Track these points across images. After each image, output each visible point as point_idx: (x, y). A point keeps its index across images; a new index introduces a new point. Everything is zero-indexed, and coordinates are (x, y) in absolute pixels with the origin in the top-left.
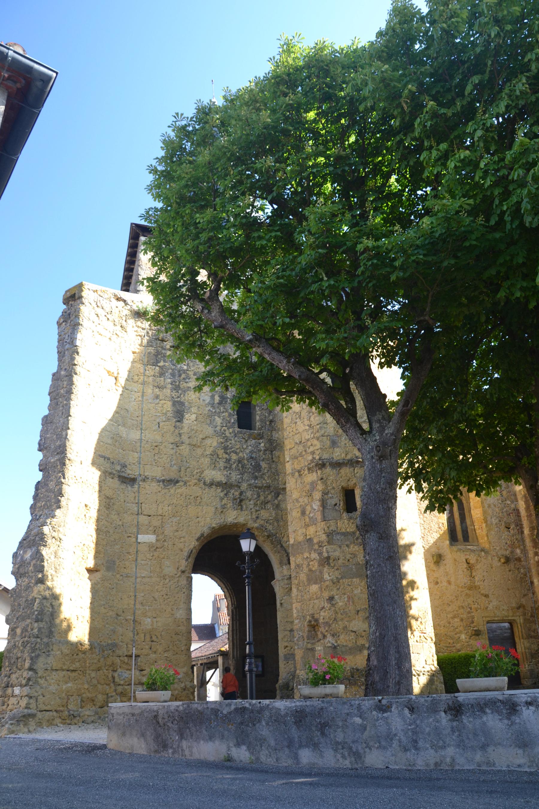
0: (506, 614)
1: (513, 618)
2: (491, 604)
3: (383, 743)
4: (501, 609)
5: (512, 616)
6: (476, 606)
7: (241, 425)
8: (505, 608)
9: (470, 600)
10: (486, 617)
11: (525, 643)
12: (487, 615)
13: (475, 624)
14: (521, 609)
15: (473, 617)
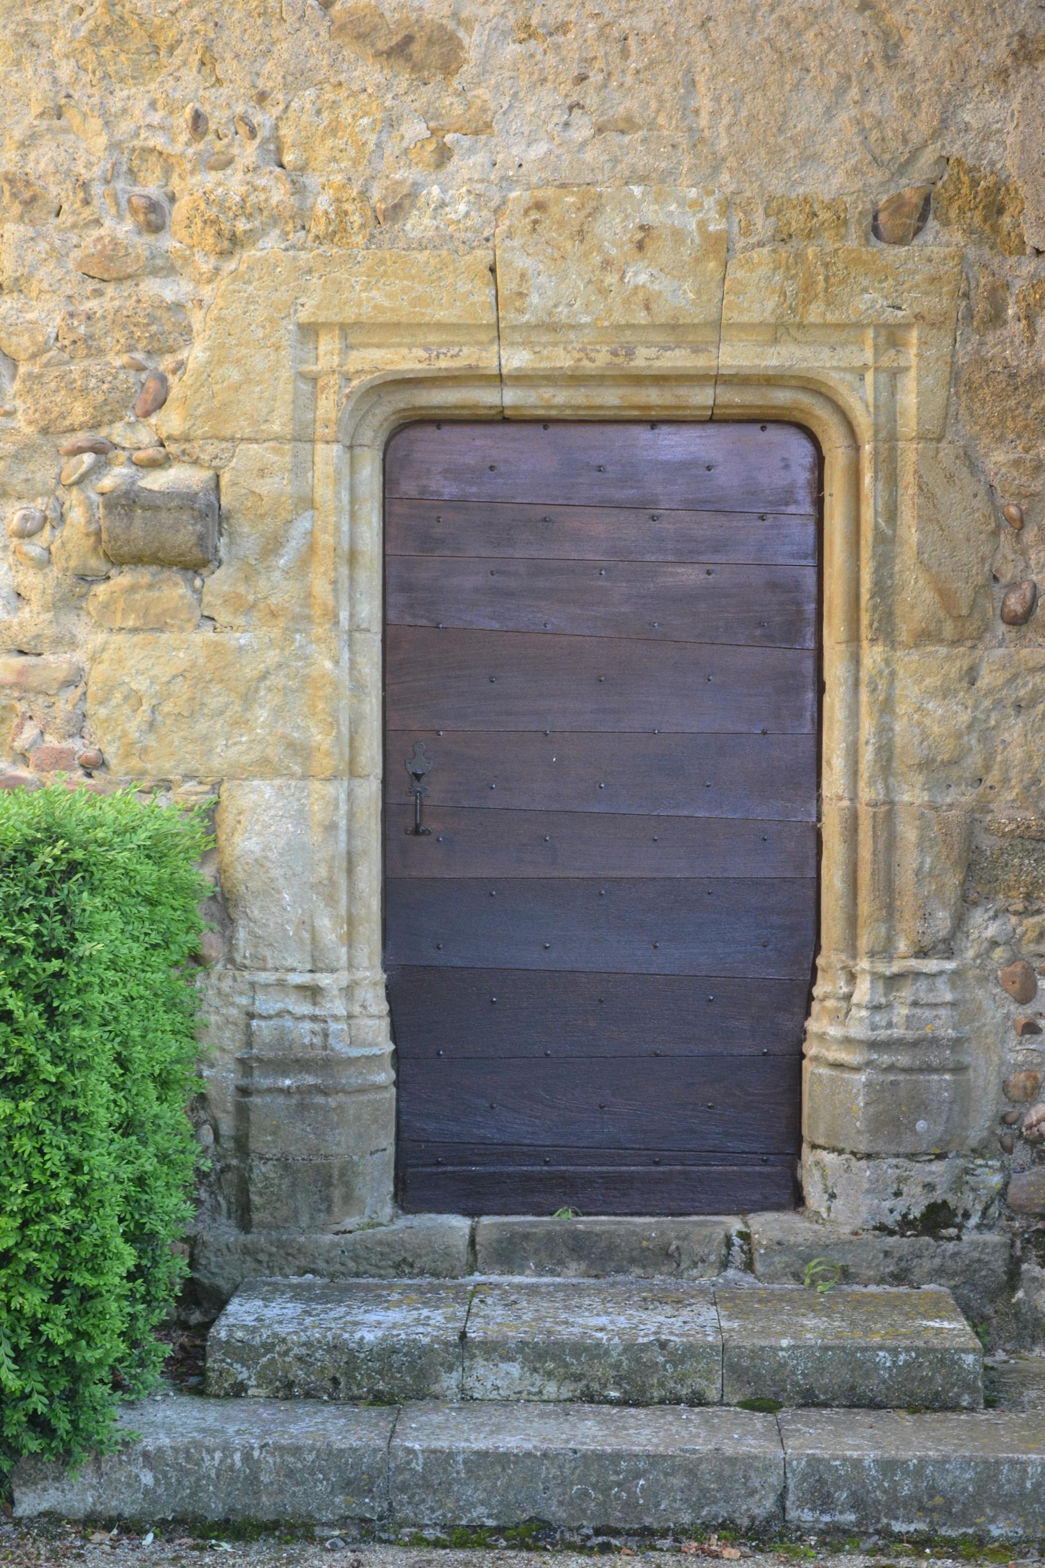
0: (681, 296)
1: (774, 358)
2: (469, 165)
3: (1021, 54)
4: (612, 229)
5: (777, 331)
6: (233, 185)
7: (195, 564)
8: (686, 211)
9: (148, 108)
10: (350, 332)
11: (909, 692)
12: (369, 298)
13: (171, 421)
14: (941, 242)
15: (161, 334)
